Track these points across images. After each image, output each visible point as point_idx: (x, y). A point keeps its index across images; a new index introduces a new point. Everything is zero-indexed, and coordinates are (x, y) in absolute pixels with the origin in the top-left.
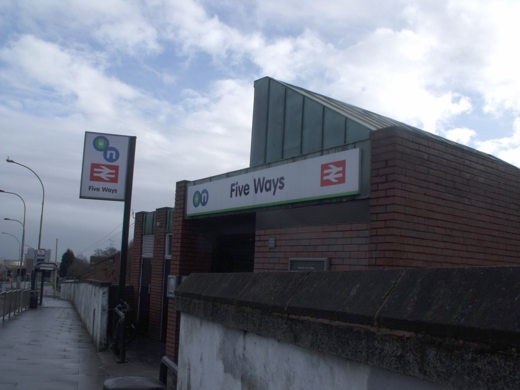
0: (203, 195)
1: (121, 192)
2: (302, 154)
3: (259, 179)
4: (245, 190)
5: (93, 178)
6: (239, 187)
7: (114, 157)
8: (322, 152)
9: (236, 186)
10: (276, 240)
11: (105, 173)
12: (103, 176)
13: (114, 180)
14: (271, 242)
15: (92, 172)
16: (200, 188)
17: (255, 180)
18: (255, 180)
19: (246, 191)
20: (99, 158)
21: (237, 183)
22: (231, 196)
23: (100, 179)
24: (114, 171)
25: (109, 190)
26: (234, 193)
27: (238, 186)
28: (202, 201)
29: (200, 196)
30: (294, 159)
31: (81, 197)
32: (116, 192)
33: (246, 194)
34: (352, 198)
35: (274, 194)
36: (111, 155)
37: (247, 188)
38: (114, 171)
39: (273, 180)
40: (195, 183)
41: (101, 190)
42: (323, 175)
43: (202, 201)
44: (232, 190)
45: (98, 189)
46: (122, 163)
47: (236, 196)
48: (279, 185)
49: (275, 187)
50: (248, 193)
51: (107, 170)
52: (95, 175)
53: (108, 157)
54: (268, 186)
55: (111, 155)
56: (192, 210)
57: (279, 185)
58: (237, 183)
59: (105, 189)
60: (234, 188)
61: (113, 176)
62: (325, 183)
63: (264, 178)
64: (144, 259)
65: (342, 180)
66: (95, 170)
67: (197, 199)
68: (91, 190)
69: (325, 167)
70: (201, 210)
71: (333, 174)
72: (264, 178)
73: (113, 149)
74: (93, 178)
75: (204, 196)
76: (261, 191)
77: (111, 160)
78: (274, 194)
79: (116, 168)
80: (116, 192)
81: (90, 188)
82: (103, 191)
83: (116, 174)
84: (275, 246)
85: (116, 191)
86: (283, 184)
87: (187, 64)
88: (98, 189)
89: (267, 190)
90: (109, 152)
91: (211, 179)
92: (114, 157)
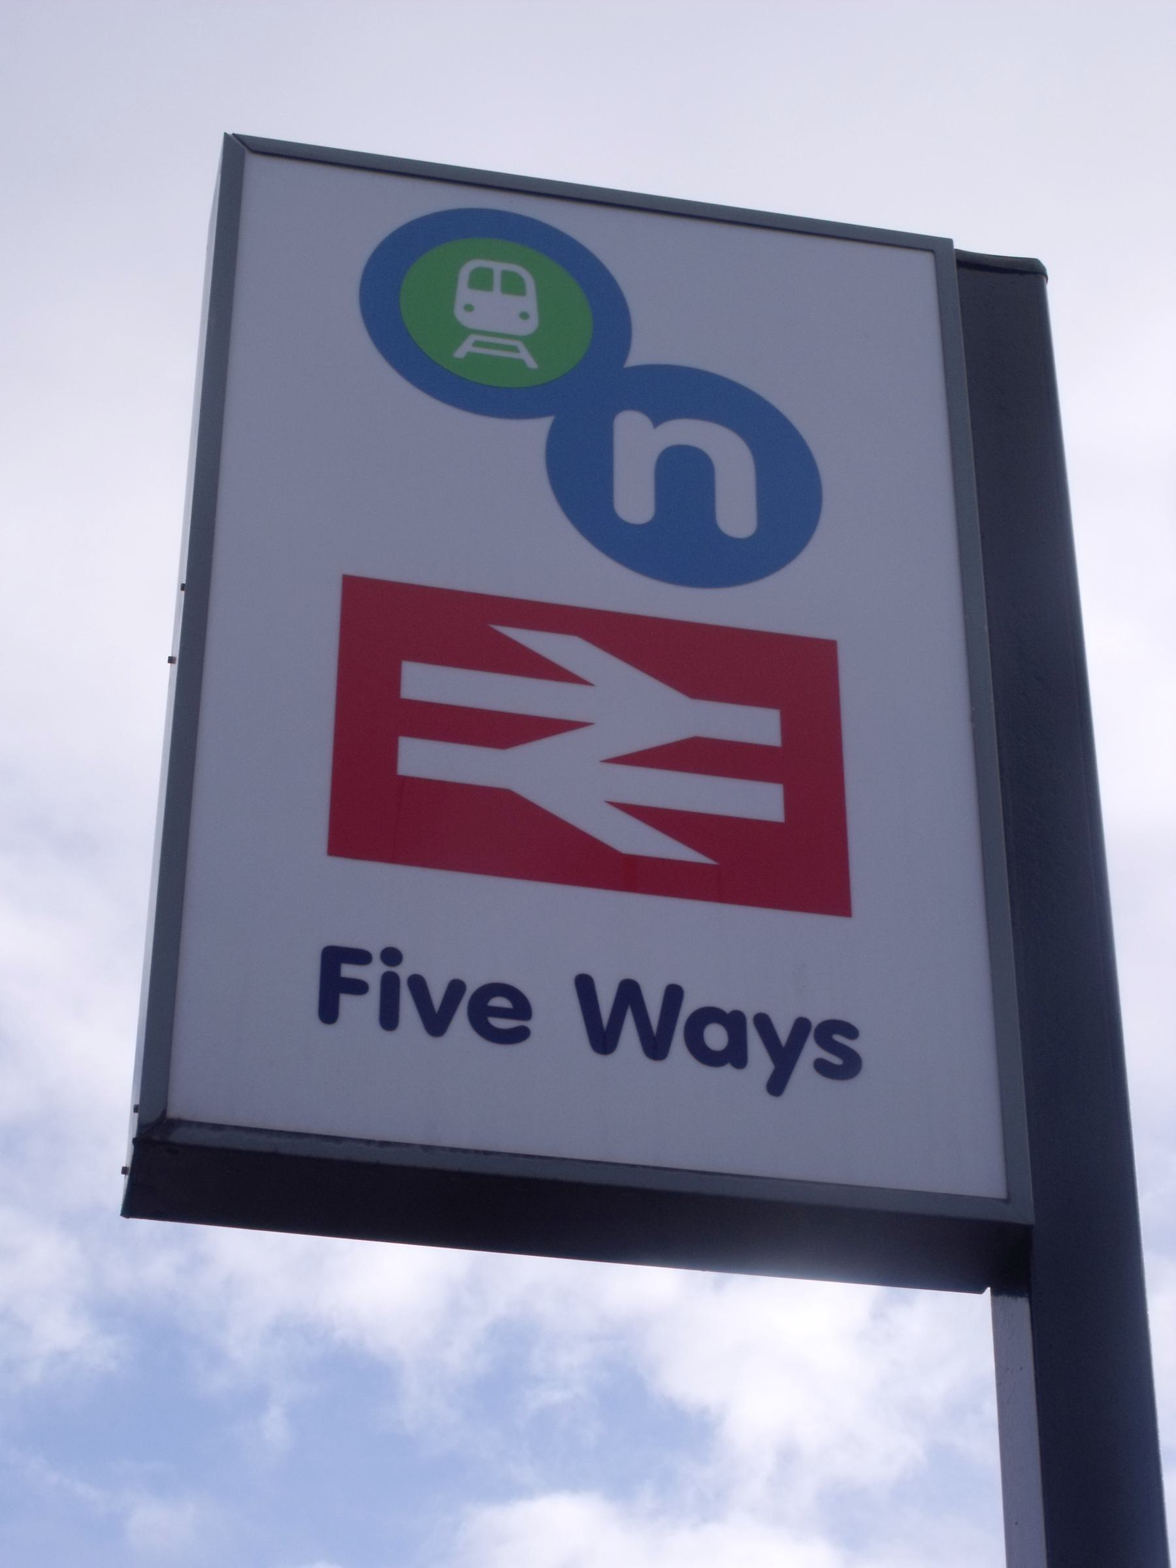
1: (934, 1116)
5: (377, 815)
7: (737, 511)
11: (598, 746)
12: (566, 782)
13: (793, 862)
15: (369, 717)
18: (585, 986)
20: (480, 512)
22: (328, 1012)
25: (720, 1037)
32: (845, 1066)
36: (684, 475)
41: (557, 1017)
45: (499, 1013)
46: (879, 591)
49: (784, 1059)
51: (637, 707)
53: (635, 499)
55: (684, 475)
57: (812, 1051)
59: (615, 1017)
60: (349, 971)
63: (674, 995)
66: (422, 682)
68: (359, 1011)
72: (674, 995)
73: (681, 391)
74: (377, 815)
77: (680, 540)
78: (776, 1085)
79: (799, 676)
80: (845, 1066)
82: (603, 1039)
83: (811, 762)
85: (836, 1047)
87: (275, 1426)
88: (499, 1013)
90: (637, 445)
92: (737, 511)
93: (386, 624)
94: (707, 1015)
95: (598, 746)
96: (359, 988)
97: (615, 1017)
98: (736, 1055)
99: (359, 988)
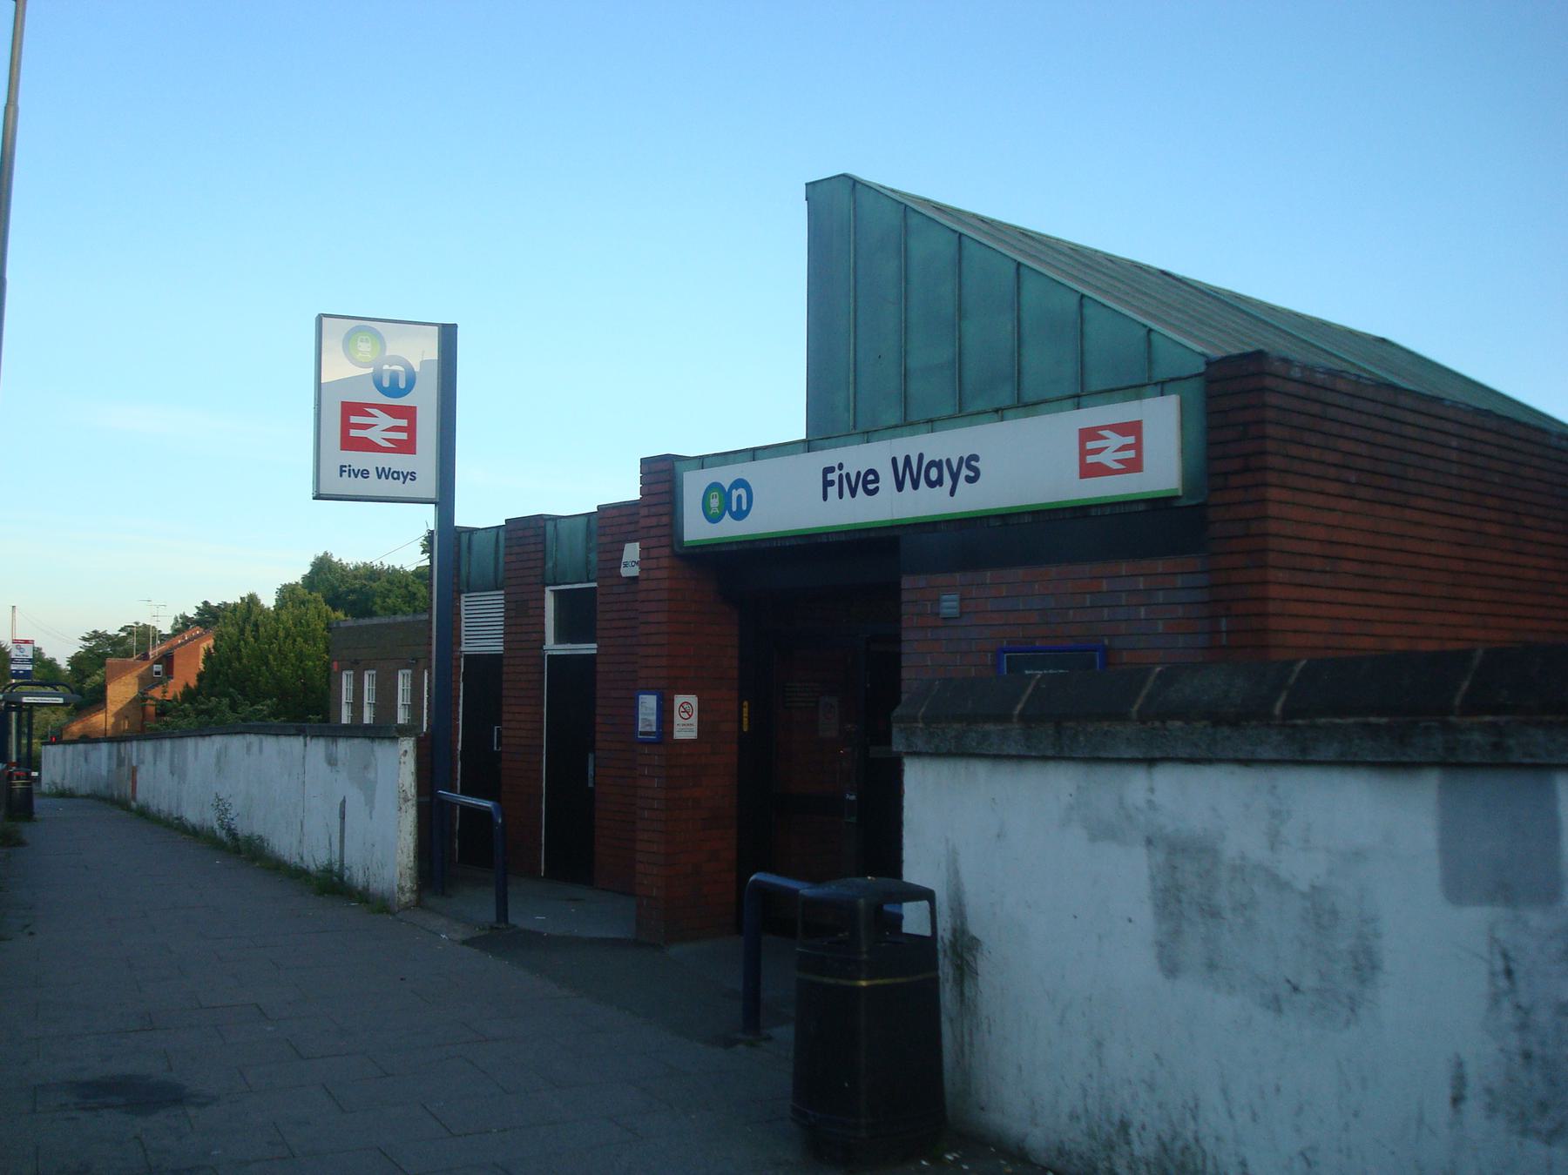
0: (735, 493)
1: (427, 483)
2: (1025, 405)
3: (907, 459)
4: (866, 483)
5: (349, 443)
6: (848, 475)
8: (1079, 398)
9: (837, 472)
10: (962, 600)
11: (380, 428)
12: (375, 435)
13: (407, 447)
14: (950, 604)
15: (346, 426)
16: (725, 476)
17: (894, 460)
18: (894, 460)
19: (871, 487)
21: (841, 466)
22: (825, 498)
23: (368, 446)
24: (404, 423)
26: (833, 491)
27: (844, 472)
28: (734, 508)
29: (726, 497)
30: (999, 413)
31: (318, 497)
32: (414, 479)
33: (871, 493)
34: (1158, 505)
35: (952, 493)
37: (871, 477)
38: (404, 423)
39: (948, 461)
40: (702, 462)
41: (373, 474)
42: (1084, 453)
43: (734, 508)
44: (827, 484)
45: (365, 474)
46: (424, 400)
47: (841, 496)
48: (965, 472)
49: (955, 477)
50: (877, 489)
51: (386, 421)
52: (354, 433)
54: (934, 474)
56: (696, 528)
57: (965, 472)
58: (841, 466)
59: (383, 473)
60: (830, 477)
61: (403, 436)
62: (1088, 471)
63: (921, 457)
64: (470, 659)
65: (1134, 466)
66: (354, 419)
67: (715, 503)
69: (1088, 434)
70: (729, 529)
71: (1111, 450)
72: (921, 457)
74: (349, 443)
75: (739, 497)
76: (915, 486)
78: (952, 493)
79: (409, 413)
80: (414, 479)
81: (342, 471)
83: (411, 430)
84: (961, 613)
86: (977, 471)
88: (365, 474)
89: (931, 484)
91: (754, 454)
93: (349, 409)
94: (932, 464)
95: (380, 428)
96: (832, 483)
97: (383, 473)
98: (939, 482)
99: (832, 483)
